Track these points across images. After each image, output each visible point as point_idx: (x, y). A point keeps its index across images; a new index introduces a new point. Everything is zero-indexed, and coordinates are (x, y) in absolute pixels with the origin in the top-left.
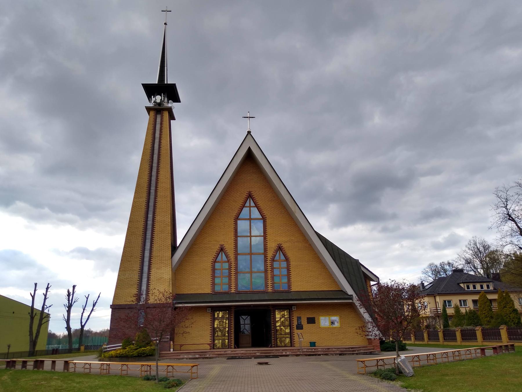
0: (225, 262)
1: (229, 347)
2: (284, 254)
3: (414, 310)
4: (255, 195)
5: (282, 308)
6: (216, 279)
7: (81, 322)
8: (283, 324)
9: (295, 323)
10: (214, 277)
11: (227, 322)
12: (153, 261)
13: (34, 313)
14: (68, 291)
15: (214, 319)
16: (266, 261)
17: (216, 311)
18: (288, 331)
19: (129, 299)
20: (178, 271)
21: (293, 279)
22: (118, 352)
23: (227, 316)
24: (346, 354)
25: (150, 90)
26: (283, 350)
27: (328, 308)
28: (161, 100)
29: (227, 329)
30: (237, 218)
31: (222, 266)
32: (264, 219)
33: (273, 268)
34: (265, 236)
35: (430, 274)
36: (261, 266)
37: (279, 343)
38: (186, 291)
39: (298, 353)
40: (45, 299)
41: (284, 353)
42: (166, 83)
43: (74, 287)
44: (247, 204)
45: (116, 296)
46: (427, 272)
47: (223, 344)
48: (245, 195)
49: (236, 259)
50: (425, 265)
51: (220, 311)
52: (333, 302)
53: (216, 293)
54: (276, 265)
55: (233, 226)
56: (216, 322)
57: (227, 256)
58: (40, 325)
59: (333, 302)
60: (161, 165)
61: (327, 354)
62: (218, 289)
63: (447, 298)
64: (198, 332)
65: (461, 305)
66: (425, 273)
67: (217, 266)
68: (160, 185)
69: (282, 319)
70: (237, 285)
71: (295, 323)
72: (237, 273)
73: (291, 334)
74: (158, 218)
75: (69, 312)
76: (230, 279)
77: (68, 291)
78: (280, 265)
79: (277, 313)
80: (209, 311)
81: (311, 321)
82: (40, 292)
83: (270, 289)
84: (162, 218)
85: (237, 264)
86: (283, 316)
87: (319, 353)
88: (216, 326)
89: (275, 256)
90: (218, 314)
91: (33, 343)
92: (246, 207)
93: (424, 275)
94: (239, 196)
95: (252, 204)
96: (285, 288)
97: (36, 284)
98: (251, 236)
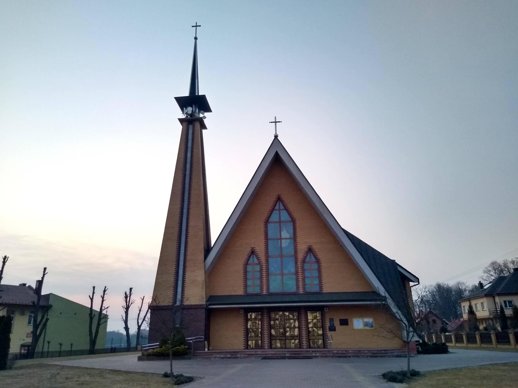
0: (256, 264)
1: (262, 347)
2: (314, 256)
3: (471, 312)
4: (284, 197)
5: (314, 309)
6: (248, 281)
7: (138, 323)
8: (315, 325)
9: (328, 325)
10: (246, 279)
11: (260, 323)
12: (188, 264)
13: (93, 314)
14: (126, 294)
15: (247, 320)
16: (296, 263)
17: (249, 312)
18: (320, 332)
19: (166, 301)
20: (211, 273)
21: (324, 281)
22: (155, 351)
23: (260, 317)
24: (377, 357)
25: (182, 102)
26: (313, 351)
27: (362, 310)
28: (192, 111)
29: (260, 330)
30: (267, 222)
31: (254, 269)
32: (293, 221)
33: (303, 270)
34: (294, 238)
35: (492, 273)
36: (291, 268)
37: (312, 345)
38: (220, 294)
39: (328, 355)
40: (103, 301)
41: (314, 355)
42: (197, 94)
43: (131, 289)
44: (277, 207)
45: (154, 298)
46: (490, 271)
47: (256, 344)
48: (274, 198)
49: (267, 261)
50: (487, 262)
51: (252, 312)
52: (363, 302)
53: (247, 295)
54: (307, 266)
55: (263, 229)
56: (249, 323)
57: (258, 259)
58: (99, 325)
59: (363, 302)
60: (194, 173)
61: (358, 356)
62: (250, 290)
63: (508, 298)
64: (231, 334)
65: (506, 306)
66: (487, 271)
67: (249, 268)
68: (192, 192)
69: (315, 321)
70: (304, 285)
71: (328, 325)
72: (268, 275)
73: (324, 335)
74: (191, 223)
75: (127, 313)
76: (261, 282)
77: (126, 294)
78: (311, 267)
79: (309, 314)
80: (242, 312)
81: (344, 322)
82: (99, 293)
83: (301, 291)
84: (195, 223)
85: (268, 266)
86: (315, 317)
87: (350, 355)
88: (249, 327)
89: (305, 257)
90: (251, 316)
91: (93, 342)
92: (276, 210)
93: (486, 275)
94: (269, 200)
95: (282, 207)
96: (316, 289)
97: (94, 288)
98: (281, 239)
